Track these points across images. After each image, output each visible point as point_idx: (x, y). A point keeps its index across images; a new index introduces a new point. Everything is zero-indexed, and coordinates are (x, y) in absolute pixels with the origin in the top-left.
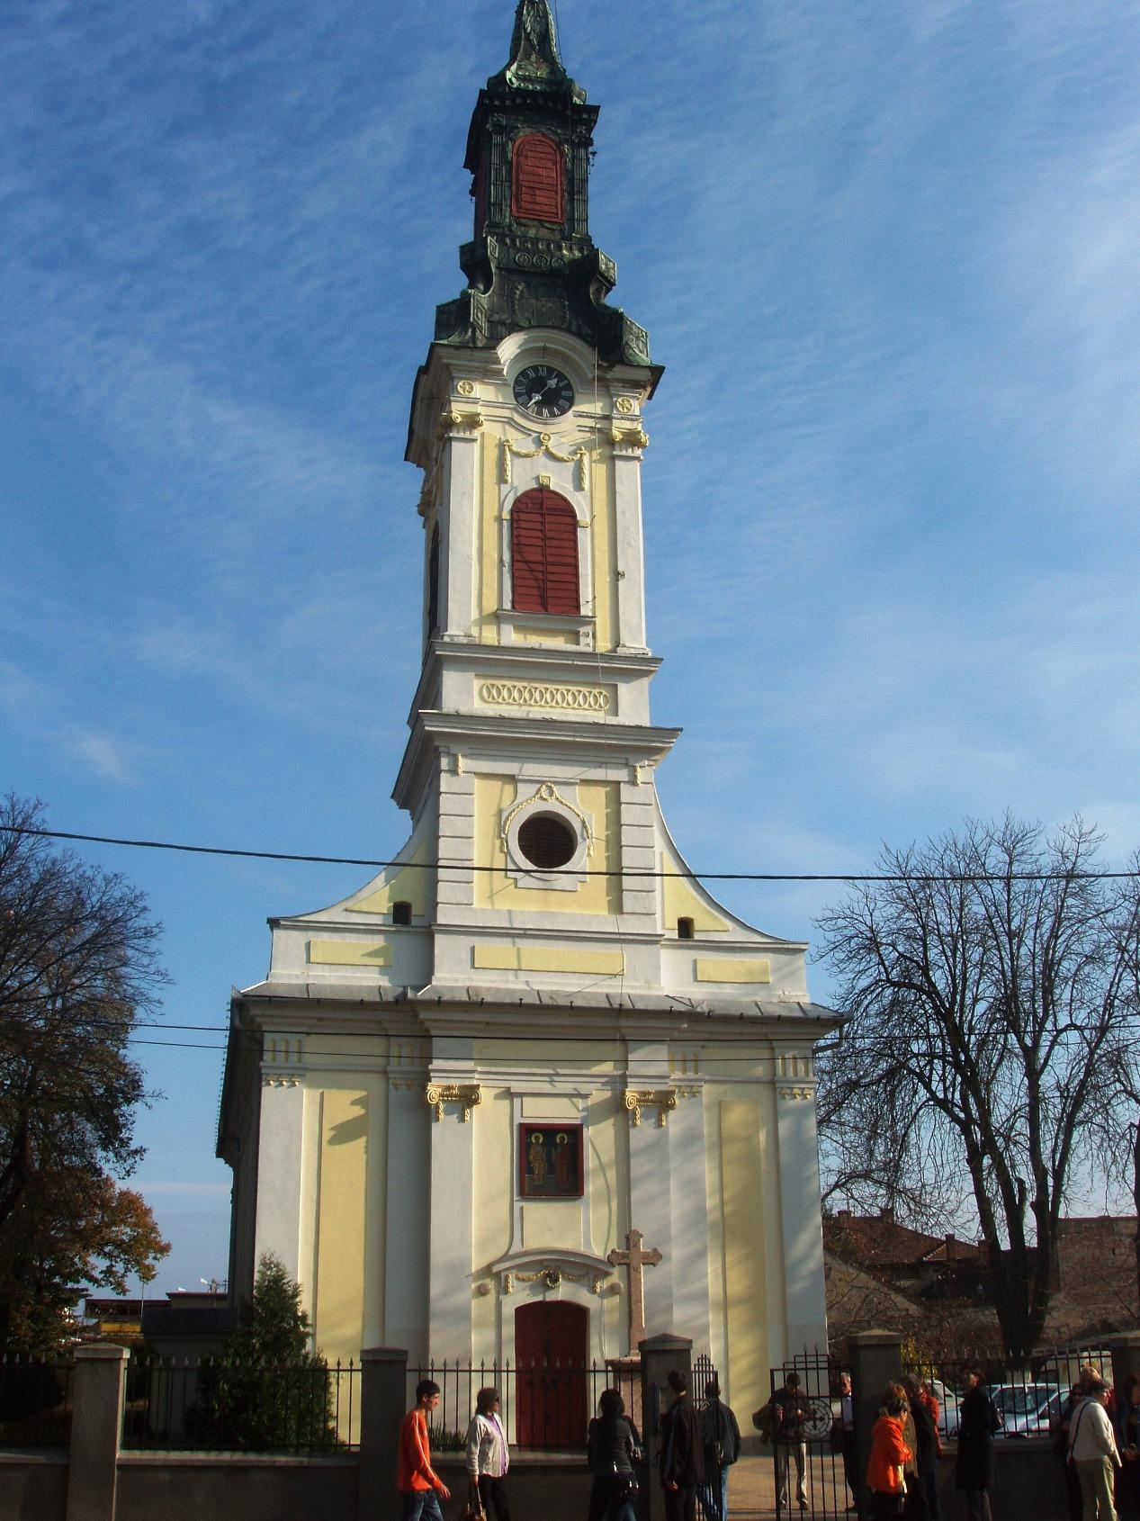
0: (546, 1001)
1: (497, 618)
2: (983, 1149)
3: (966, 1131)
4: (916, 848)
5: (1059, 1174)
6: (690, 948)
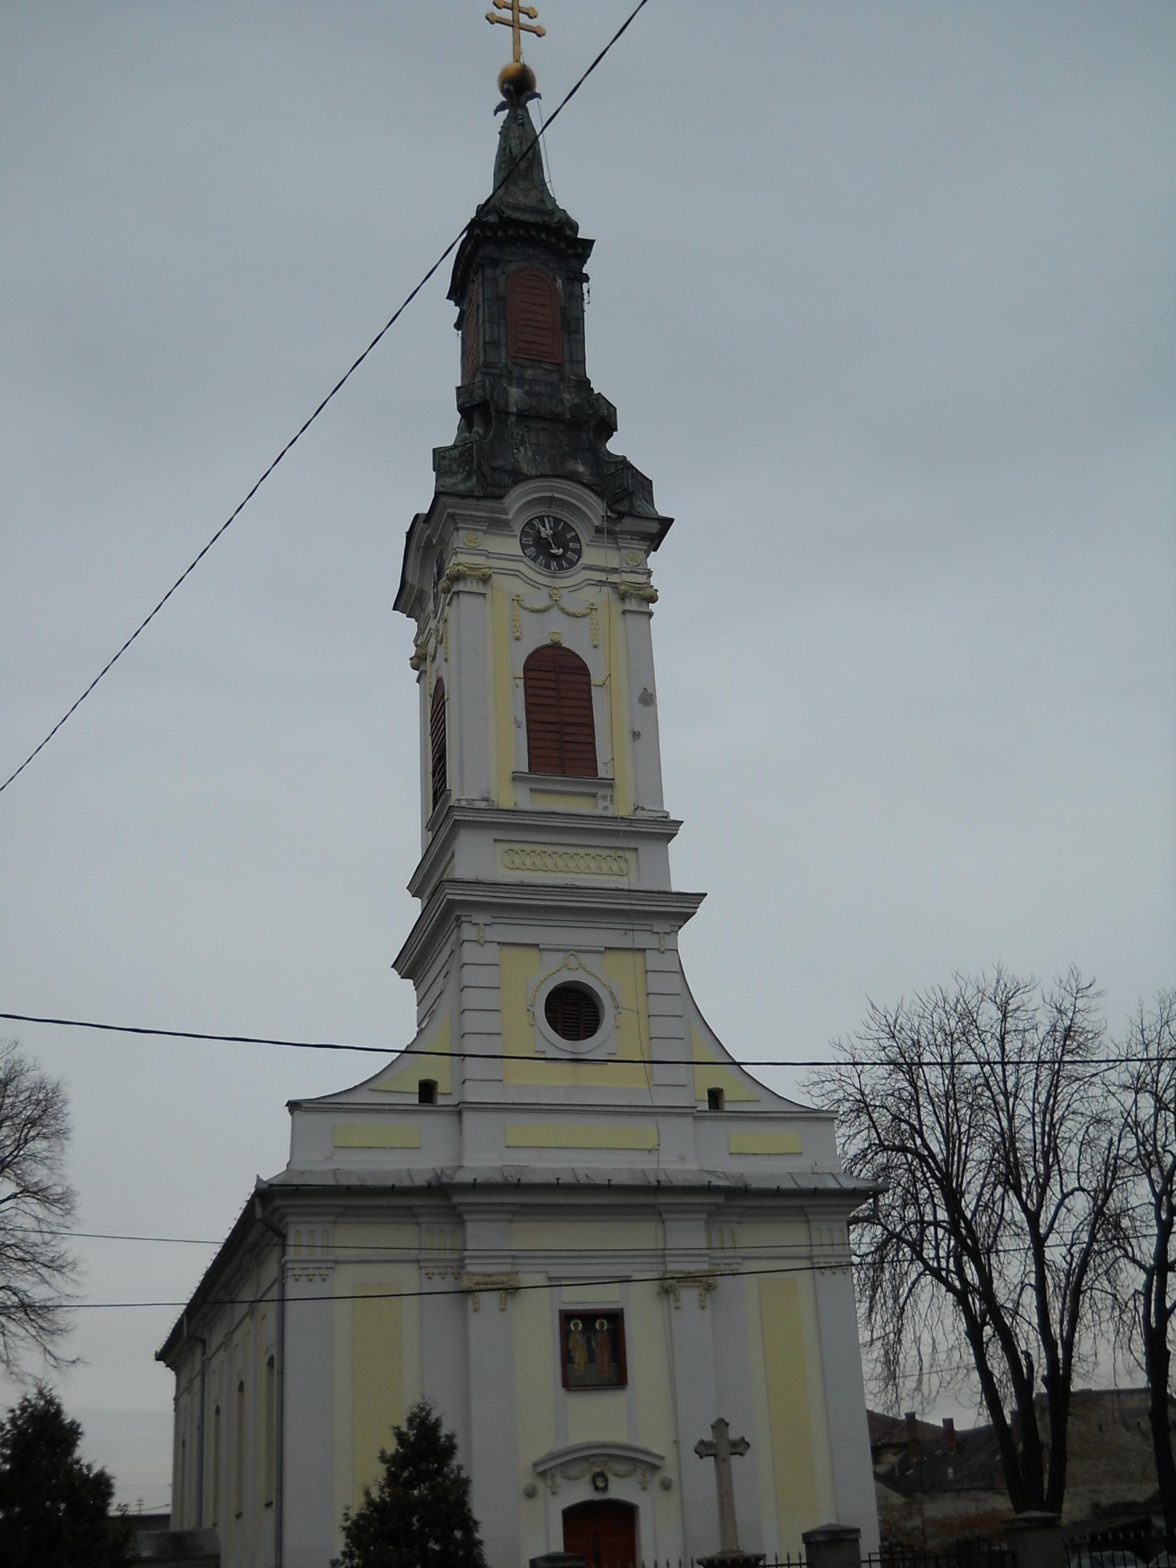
0: (583, 1180)
1: (517, 778)
2: (983, 1315)
3: (962, 1299)
4: (906, 1008)
5: (1069, 1345)
6: (721, 1119)
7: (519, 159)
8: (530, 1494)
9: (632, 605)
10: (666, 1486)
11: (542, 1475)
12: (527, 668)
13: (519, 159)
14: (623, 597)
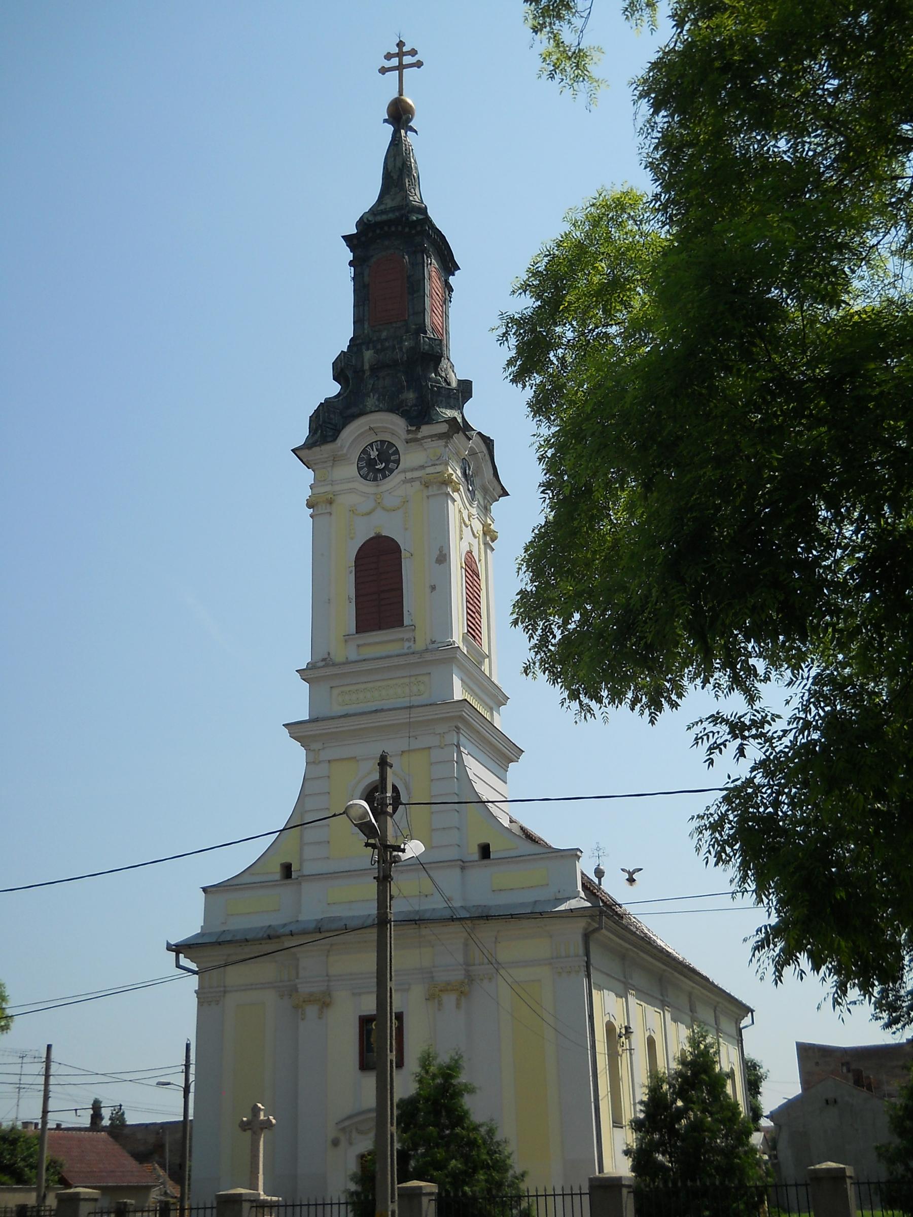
7: (398, 170)
8: (336, 1143)
9: (433, 490)
10: (336, 1143)
11: (343, 1130)
12: (357, 558)
13: (398, 170)
14: (427, 485)
